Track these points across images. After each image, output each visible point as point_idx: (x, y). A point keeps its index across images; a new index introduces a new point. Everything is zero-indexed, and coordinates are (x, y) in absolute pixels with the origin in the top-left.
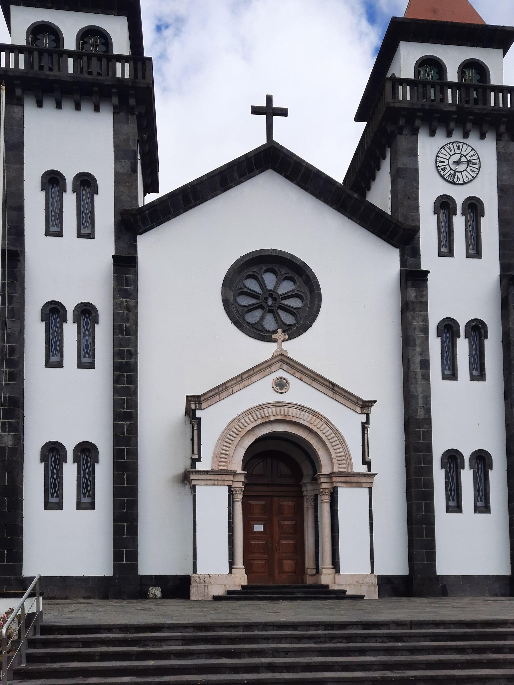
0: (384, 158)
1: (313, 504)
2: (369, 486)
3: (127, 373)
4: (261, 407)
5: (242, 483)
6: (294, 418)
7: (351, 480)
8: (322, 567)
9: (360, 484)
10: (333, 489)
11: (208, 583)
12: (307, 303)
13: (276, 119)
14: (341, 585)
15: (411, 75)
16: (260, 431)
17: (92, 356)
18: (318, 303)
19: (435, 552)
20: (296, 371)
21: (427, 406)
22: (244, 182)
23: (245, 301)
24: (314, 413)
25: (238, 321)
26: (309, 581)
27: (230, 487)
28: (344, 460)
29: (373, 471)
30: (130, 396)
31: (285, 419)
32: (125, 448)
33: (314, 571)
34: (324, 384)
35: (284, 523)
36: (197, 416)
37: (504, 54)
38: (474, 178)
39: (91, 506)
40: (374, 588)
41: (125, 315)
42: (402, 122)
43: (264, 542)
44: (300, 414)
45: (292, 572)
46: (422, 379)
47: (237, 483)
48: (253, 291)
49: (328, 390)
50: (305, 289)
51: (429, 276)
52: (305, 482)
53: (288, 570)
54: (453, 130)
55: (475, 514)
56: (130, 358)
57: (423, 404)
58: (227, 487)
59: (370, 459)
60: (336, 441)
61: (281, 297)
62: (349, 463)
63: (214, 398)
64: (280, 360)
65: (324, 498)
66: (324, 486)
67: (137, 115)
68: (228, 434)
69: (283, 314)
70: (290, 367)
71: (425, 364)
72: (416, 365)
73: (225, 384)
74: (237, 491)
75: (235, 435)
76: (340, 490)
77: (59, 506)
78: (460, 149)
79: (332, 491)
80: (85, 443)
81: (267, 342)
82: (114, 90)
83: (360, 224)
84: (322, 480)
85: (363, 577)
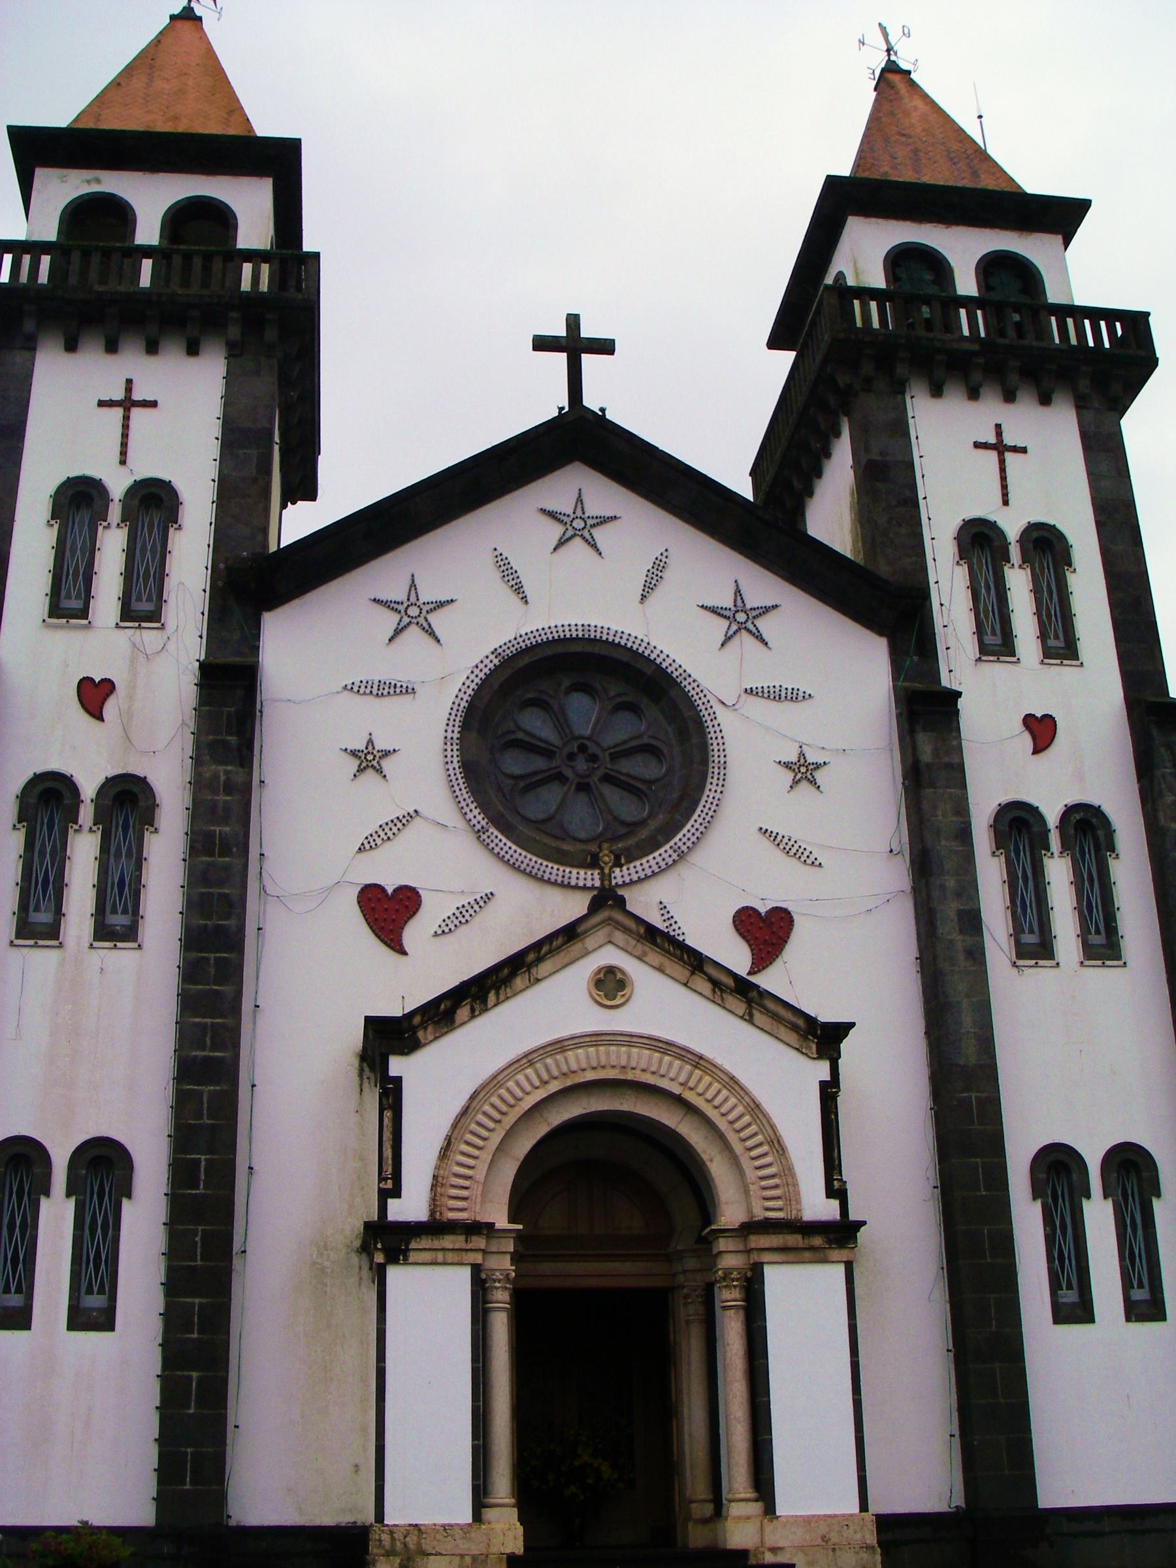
0: (838, 435)
1: (701, 1309)
3: (218, 955)
4: (559, 1046)
5: (508, 1257)
8: (730, 1496)
10: (751, 1270)
13: (589, 361)
15: (877, 280)
17: (133, 911)
19: (1031, 1440)
23: (515, 764)
26: (697, 1537)
27: (476, 1269)
28: (776, 1187)
30: (222, 1016)
31: (622, 1077)
32: (203, 1157)
33: (709, 1509)
36: (393, 1071)
37: (1067, 243)
39: (104, 1321)
42: (867, 368)
44: (660, 1062)
48: (540, 739)
51: (961, 703)
52: (679, 1247)
54: (981, 386)
60: (710, 1084)
62: (792, 1194)
68: (473, 1121)
69: (611, 793)
71: (972, 921)
74: (495, 1281)
75: (491, 1125)
76: (768, 1270)
79: (749, 1274)
82: (234, 315)
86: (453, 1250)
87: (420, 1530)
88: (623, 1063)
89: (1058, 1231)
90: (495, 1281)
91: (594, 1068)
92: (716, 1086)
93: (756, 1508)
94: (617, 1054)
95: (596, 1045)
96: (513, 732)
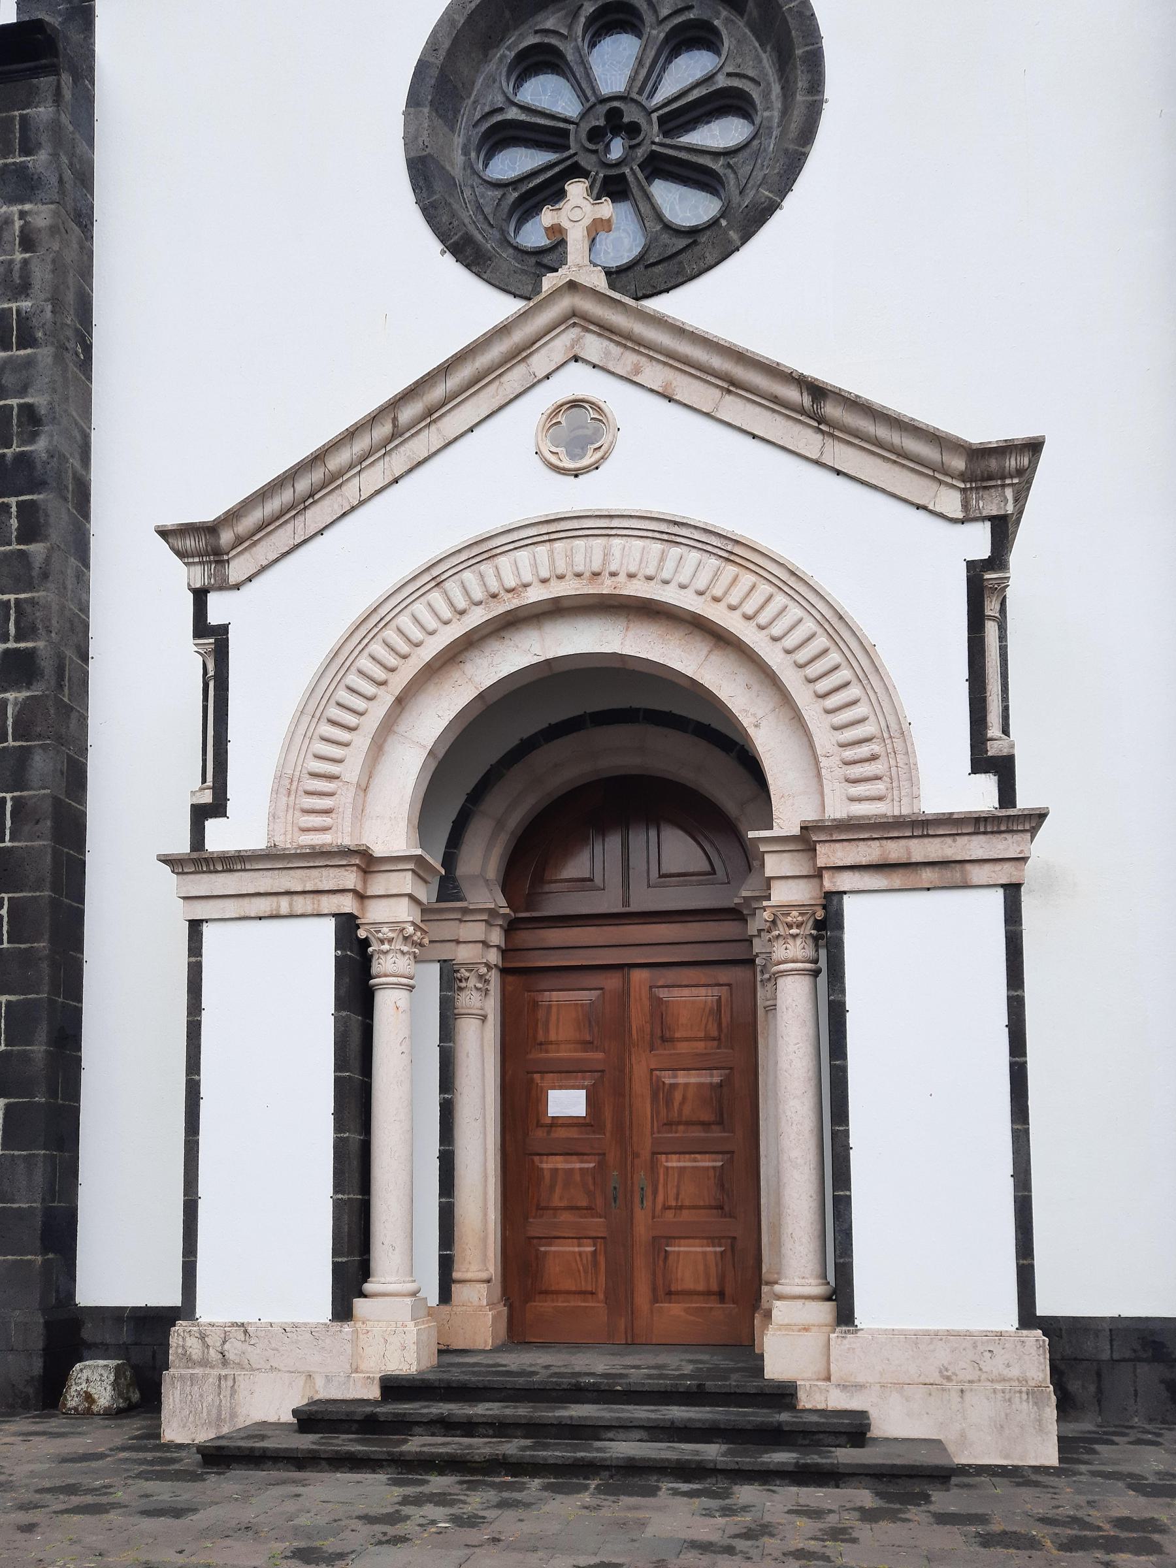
2: (1005, 874)
6: (635, 581)
7: (909, 853)
9: (955, 875)
10: (824, 907)
11: (240, 1365)
12: (770, 119)
14: (859, 1387)
16: (491, 664)
18: (810, 98)
20: (643, 360)
24: (729, 548)
25: (468, 240)
27: (347, 926)
28: (874, 758)
29: (1025, 800)
30: (30, 587)
32: (8, 796)
34: (775, 399)
35: (672, 1081)
40: (1036, 1404)
41: (17, 267)
43: (592, 1165)
45: (708, 1293)
47: (384, 902)
49: (798, 428)
50: (761, 61)
53: (689, 1284)
56: (33, 437)
58: (331, 924)
59: (1012, 746)
61: (655, 116)
63: (281, 532)
65: (780, 951)
66: (782, 894)
70: (618, 344)
73: (318, 458)
74: (382, 941)
76: (850, 905)
79: (820, 914)
84: (774, 865)
85: (975, 1347)
86: (304, 892)
87: (246, 1332)
88: (596, 567)
90: (382, 941)
91: (544, 581)
92: (765, 589)
93: (824, 1312)
95: (549, 541)
96: (501, 110)
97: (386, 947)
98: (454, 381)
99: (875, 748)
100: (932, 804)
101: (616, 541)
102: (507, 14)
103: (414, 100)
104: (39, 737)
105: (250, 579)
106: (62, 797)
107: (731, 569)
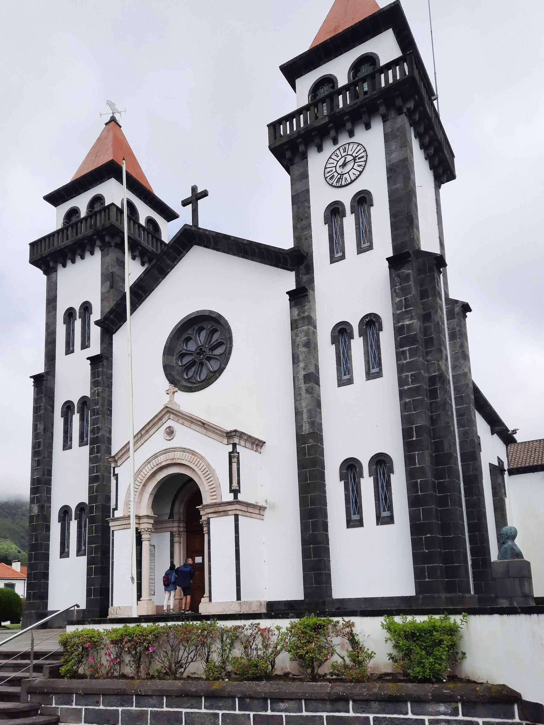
2: (234, 512)
9: (226, 513)
21: (311, 420)
22: (176, 264)
28: (215, 491)
38: (361, 172)
39: (390, 520)
46: (306, 393)
55: (378, 526)
56: (98, 433)
57: (308, 418)
60: (197, 459)
64: (167, 412)
67: (114, 246)
72: (301, 381)
77: (360, 523)
78: (347, 151)
80: (383, 455)
81: (194, 392)
82: (95, 237)
83: (261, 262)
89: (355, 489)
90: (142, 532)
94: (171, 455)
97: (143, 533)
98: (150, 426)
99: (215, 489)
100: (225, 500)
101: (176, 452)
102: (181, 332)
103: (164, 354)
104: (99, 492)
105: (121, 465)
106: (104, 503)
107: (193, 456)
